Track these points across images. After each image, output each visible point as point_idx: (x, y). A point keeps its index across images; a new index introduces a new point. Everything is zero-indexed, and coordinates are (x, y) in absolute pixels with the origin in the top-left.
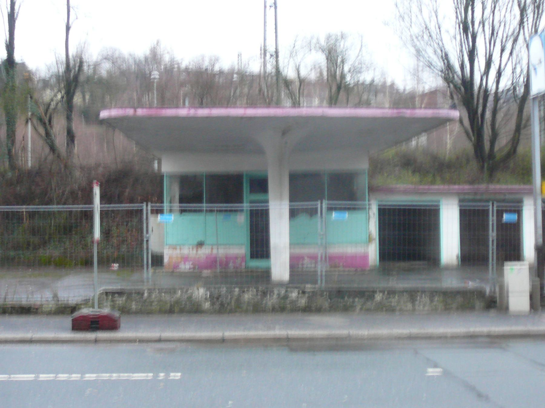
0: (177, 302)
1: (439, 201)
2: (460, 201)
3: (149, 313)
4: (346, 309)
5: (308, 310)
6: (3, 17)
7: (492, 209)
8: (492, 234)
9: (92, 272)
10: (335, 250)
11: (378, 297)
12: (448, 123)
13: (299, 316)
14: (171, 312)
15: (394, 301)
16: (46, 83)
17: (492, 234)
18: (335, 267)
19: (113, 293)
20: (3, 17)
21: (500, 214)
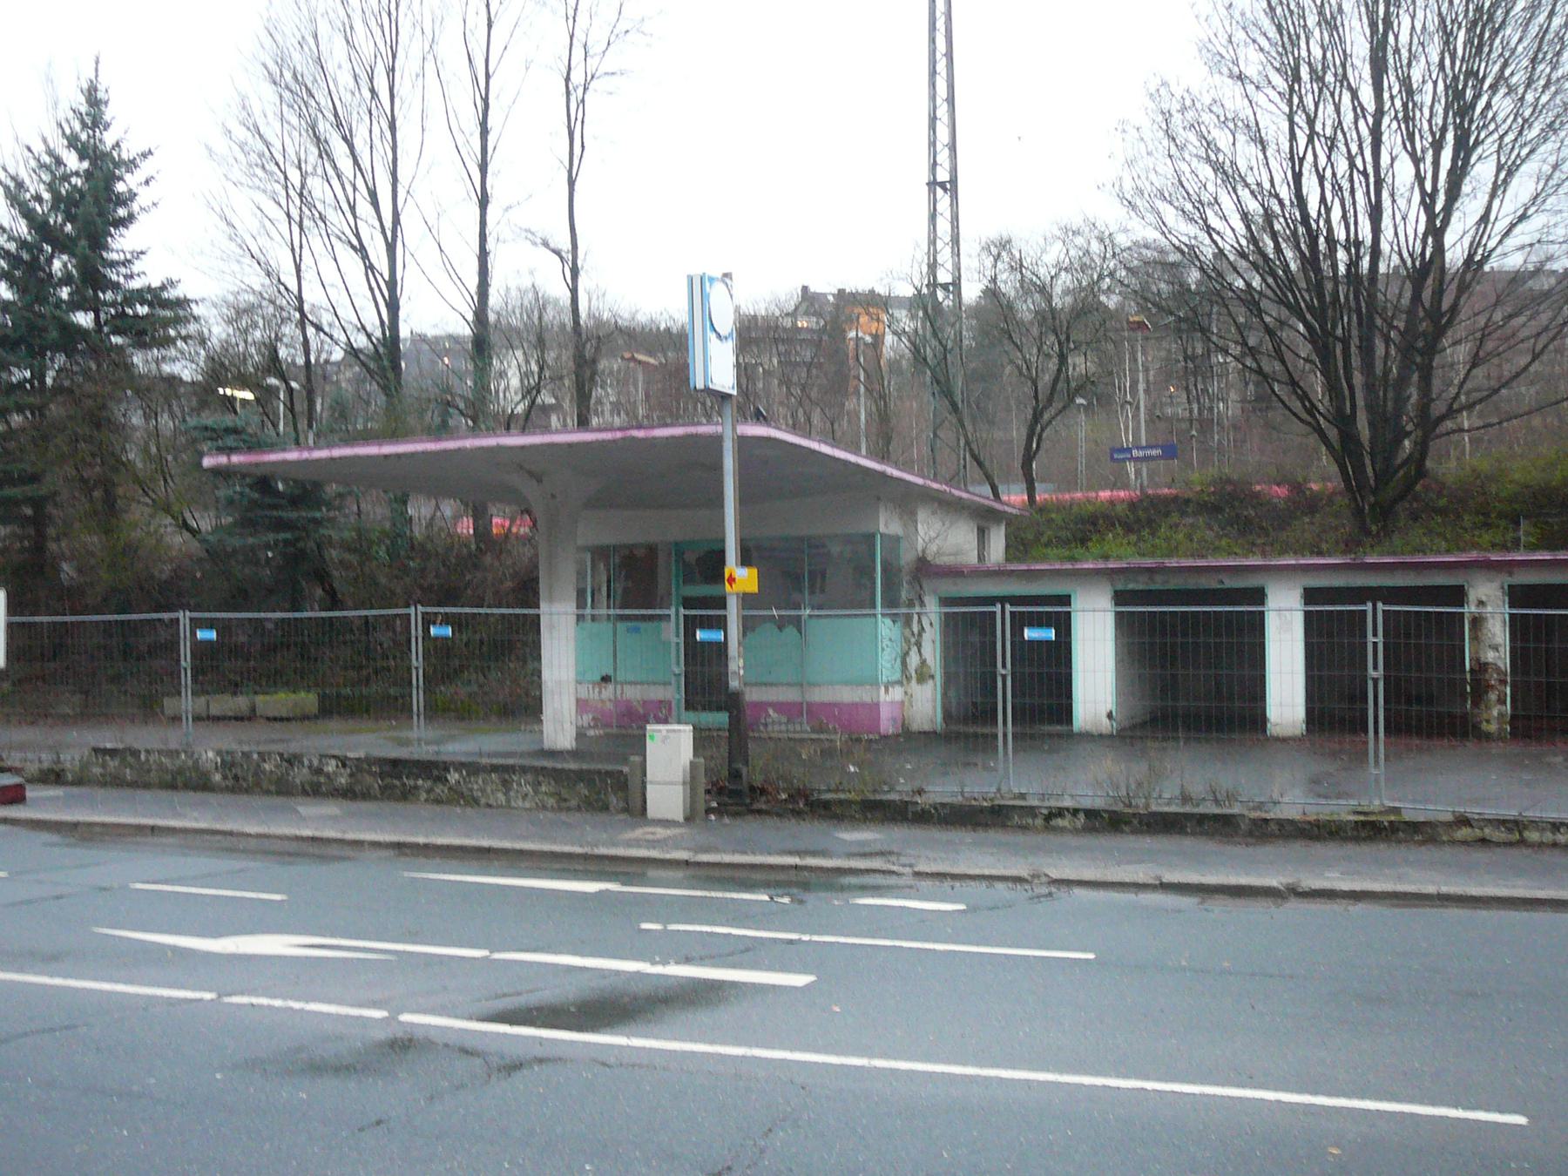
0: (180, 771)
1: (1065, 600)
2: (1120, 598)
3: (147, 786)
4: (406, 795)
5: (348, 794)
6: (571, 183)
7: (1002, 615)
8: (417, 661)
9: (1361, 757)
10: (820, 695)
11: (453, 777)
12: (1465, 413)
13: (128, 792)
14: (172, 786)
15: (477, 783)
16: (793, 314)
17: (417, 661)
18: (821, 731)
19: (105, 751)
20: (571, 183)
21: (1017, 630)
